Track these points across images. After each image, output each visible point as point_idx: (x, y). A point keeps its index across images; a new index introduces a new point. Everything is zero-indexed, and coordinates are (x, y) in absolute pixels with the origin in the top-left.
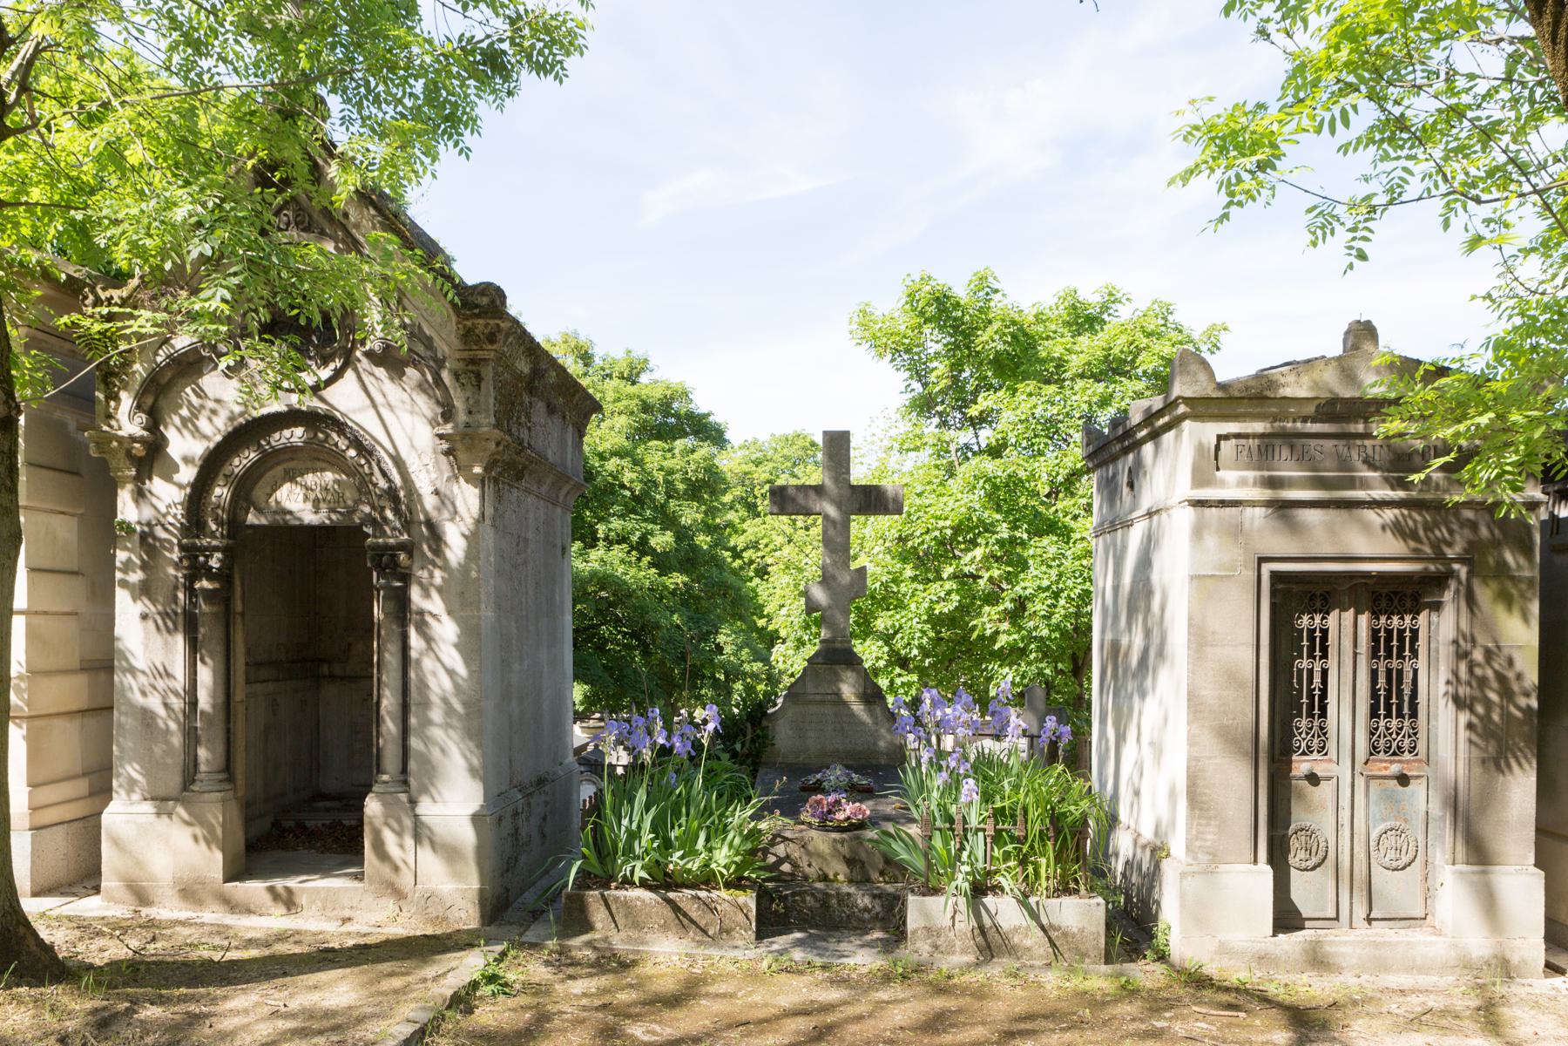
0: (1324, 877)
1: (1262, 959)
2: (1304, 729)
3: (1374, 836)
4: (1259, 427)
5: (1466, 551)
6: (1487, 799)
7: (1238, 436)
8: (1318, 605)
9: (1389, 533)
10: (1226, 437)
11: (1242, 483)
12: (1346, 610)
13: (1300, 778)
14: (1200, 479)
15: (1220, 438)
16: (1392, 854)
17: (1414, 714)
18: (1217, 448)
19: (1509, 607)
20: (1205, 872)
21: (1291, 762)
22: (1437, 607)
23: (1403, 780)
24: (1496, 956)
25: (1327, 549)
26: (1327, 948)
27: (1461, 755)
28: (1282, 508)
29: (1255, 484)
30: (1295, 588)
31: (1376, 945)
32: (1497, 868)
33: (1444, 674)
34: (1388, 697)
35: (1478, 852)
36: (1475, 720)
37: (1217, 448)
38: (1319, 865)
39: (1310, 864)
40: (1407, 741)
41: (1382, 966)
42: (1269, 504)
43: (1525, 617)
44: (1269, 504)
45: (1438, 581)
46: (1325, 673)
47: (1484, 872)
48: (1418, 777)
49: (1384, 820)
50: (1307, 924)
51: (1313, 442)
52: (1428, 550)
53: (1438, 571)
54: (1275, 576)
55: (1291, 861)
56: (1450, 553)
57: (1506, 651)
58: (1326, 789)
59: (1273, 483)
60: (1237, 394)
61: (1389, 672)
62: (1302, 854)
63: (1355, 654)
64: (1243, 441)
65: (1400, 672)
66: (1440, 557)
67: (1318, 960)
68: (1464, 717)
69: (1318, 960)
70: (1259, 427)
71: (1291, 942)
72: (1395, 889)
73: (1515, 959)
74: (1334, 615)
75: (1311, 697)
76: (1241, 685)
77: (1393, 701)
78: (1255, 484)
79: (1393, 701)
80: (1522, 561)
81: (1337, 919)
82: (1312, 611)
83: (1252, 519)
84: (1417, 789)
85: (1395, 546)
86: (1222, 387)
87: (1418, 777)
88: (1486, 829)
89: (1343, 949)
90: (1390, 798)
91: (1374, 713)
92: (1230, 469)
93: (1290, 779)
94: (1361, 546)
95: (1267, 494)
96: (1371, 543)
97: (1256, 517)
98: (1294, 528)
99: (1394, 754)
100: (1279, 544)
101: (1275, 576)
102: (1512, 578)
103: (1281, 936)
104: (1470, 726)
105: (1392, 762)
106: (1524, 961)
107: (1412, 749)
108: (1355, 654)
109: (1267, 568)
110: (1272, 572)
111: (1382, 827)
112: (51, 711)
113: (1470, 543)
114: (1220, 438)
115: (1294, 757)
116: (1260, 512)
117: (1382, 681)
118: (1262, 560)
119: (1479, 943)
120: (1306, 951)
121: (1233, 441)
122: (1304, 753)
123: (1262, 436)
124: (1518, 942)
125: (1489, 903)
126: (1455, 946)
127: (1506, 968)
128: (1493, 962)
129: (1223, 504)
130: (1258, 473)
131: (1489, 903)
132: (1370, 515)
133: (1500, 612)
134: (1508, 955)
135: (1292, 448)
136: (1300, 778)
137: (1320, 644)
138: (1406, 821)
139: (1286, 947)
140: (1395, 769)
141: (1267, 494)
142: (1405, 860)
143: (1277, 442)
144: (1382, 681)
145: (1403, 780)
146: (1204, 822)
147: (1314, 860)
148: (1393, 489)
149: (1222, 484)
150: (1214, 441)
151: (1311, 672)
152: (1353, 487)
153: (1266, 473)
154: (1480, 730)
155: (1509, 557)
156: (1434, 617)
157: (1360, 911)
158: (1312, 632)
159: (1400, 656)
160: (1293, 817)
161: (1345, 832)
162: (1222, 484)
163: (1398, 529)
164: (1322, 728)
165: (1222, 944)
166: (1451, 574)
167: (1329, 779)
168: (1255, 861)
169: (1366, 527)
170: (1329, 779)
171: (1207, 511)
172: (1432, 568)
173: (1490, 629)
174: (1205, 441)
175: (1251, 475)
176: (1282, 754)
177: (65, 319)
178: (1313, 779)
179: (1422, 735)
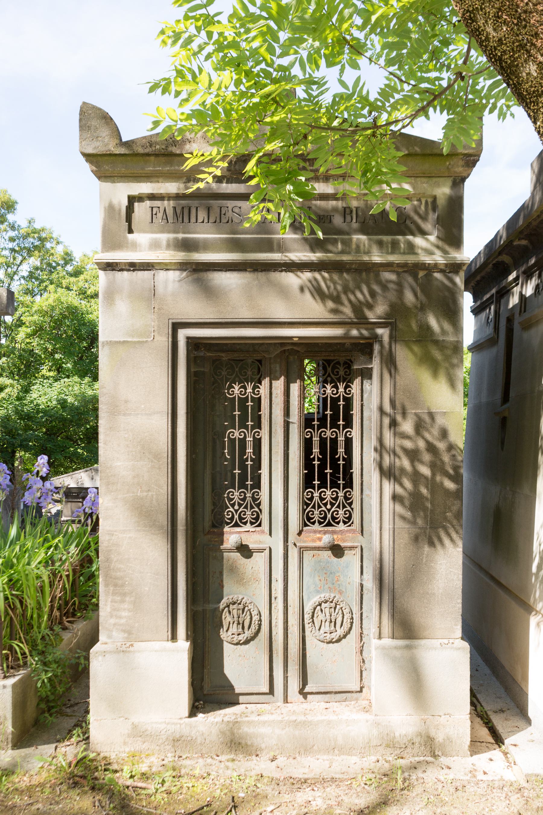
0: (257, 652)
1: (177, 741)
2: (236, 499)
3: (308, 609)
4: (172, 187)
5: (388, 316)
6: (416, 572)
7: (152, 197)
8: (342, 373)
9: (308, 295)
10: (140, 198)
11: (155, 245)
12: (277, 379)
13: (230, 550)
14: (110, 241)
15: (132, 200)
16: (326, 627)
17: (349, 484)
18: (130, 209)
19: (435, 374)
20: (117, 651)
21: (222, 534)
22: (367, 374)
23: (337, 550)
24: (420, 734)
25: (245, 315)
26: (246, 729)
27: (387, 526)
28: (198, 270)
29: (168, 246)
30: (225, 357)
31: (296, 724)
32: (423, 642)
33: (371, 442)
34: (322, 467)
35: (406, 628)
36: (399, 490)
37: (130, 209)
38: (253, 638)
39: (243, 638)
40: (341, 512)
41: (305, 748)
42: (183, 266)
43: (452, 384)
44: (183, 266)
45: (365, 348)
46: (258, 444)
47: (409, 647)
48: (352, 548)
49: (318, 592)
50: (242, 699)
51: (231, 204)
52: (348, 311)
53: (362, 337)
54: (192, 342)
55: (223, 635)
56: (372, 317)
57: (440, 421)
58: (259, 561)
59: (187, 246)
60: (141, 150)
61: (323, 442)
62: (234, 629)
63: (287, 425)
64: (157, 203)
65: (334, 441)
66: (361, 320)
67: (236, 744)
68: (388, 488)
69: (236, 744)
70: (172, 187)
71: (212, 722)
72: (330, 661)
73: (440, 737)
74: (266, 382)
75: (243, 467)
76: (157, 456)
77: (327, 469)
78: (168, 246)
79: (327, 469)
80: (447, 326)
81: (271, 692)
82: (243, 380)
83: (166, 282)
84: (351, 559)
85: (316, 309)
86: (128, 144)
87: (352, 548)
88: (413, 604)
89: (263, 730)
90: (326, 573)
91: (308, 482)
92: (144, 232)
93: (221, 552)
94: (279, 311)
95: (180, 256)
96: (293, 307)
97: (170, 279)
98: (209, 292)
99: (329, 524)
100: (193, 308)
101: (192, 342)
102: (436, 342)
103: (201, 716)
104: (395, 498)
105: (325, 533)
106: (449, 739)
107: (348, 520)
108: (287, 425)
109: (183, 334)
110: (188, 338)
111: (316, 599)
112: (273, 416)
113: (392, 306)
114: (132, 200)
115: (226, 529)
116: (174, 275)
117: (316, 450)
118: (176, 326)
119: (401, 719)
120: (223, 733)
121: (148, 203)
122: (236, 525)
123: (178, 197)
124: (443, 720)
125: (415, 682)
126: (378, 724)
127: (432, 748)
128: (417, 740)
129: (133, 267)
130: (172, 236)
131: (415, 682)
132: (292, 280)
133: (424, 375)
134: (432, 734)
135: (209, 209)
136: (230, 550)
137: (251, 414)
138: (341, 592)
139: (202, 728)
140: (326, 539)
141: (180, 256)
142: (340, 632)
143: (194, 203)
144: (316, 450)
145: (337, 550)
146: (118, 598)
147: (248, 634)
148: (313, 250)
149: (134, 246)
150: (125, 202)
151: (243, 442)
152: (271, 250)
153: (181, 236)
154: (407, 503)
155: (433, 322)
156: (366, 384)
157: (294, 684)
158: (243, 401)
159: (334, 425)
160: (226, 590)
161: (278, 605)
162: (134, 246)
163: (319, 293)
164: (254, 499)
165: (135, 726)
166: (376, 338)
167: (261, 551)
168: (174, 637)
169: (283, 292)
170: (261, 551)
171: (118, 275)
172: (354, 332)
173: (415, 395)
174: (115, 202)
175: (164, 237)
176: (214, 526)
177: (402, 245)
178: (245, 550)
179: (356, 506)
